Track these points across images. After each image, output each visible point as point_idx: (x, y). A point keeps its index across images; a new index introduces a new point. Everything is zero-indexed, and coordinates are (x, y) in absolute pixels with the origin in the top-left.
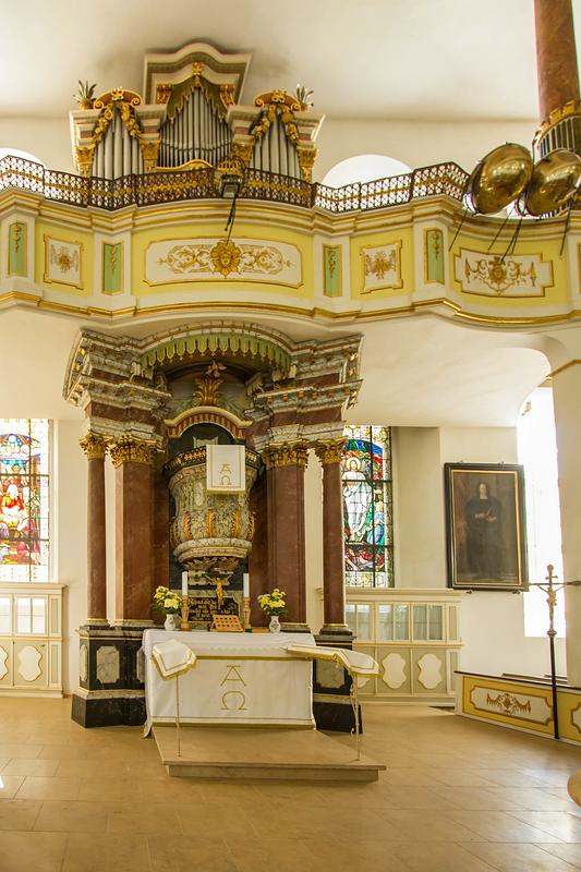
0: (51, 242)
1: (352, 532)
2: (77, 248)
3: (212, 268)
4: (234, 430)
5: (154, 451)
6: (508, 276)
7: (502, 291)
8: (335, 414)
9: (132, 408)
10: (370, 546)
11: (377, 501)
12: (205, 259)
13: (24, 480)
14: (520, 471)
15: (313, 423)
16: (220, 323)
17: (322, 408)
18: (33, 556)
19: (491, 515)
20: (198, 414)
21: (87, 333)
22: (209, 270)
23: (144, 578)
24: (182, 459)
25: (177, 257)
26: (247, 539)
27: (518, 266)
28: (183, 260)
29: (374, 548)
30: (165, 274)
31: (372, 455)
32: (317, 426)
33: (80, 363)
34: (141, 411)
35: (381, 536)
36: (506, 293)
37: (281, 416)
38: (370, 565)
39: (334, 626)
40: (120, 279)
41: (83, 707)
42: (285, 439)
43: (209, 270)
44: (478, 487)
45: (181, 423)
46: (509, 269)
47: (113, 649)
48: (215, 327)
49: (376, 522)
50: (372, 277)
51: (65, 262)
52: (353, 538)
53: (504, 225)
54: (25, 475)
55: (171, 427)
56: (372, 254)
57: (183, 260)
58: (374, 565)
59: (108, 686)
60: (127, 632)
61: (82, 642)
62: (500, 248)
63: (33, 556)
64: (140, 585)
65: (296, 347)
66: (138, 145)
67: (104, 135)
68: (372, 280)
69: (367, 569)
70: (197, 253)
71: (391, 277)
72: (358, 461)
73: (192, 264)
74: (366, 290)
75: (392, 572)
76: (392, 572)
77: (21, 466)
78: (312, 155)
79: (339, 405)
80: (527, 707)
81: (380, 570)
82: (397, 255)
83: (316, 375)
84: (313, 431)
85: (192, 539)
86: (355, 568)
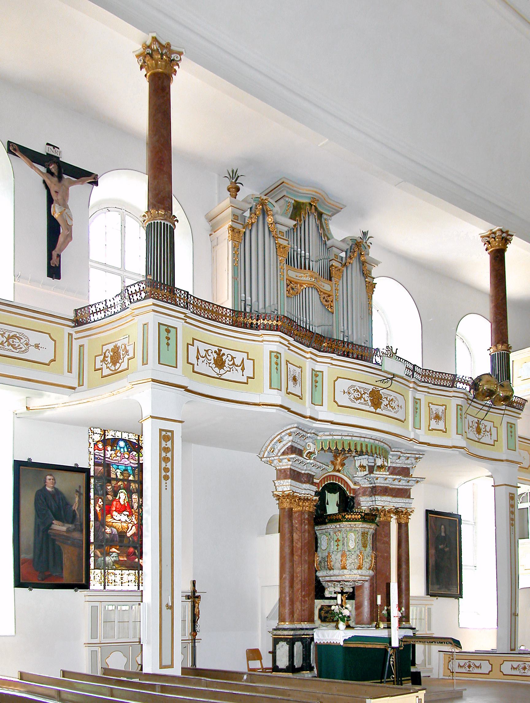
3: (370, 404)
6: (482, 431)
8: (407, 493)
12: (366, 396)
14: (460, 520)
19: (446, 546)
25: (352, 392)
28: (356, 394)
37: (380, 488)
42: (382, 504)
44: (441, 527)
50: (433, 422)
54: (134, 481)
57: (356, 394)
59: (282, 670)
79: (410, 487)
80: (479, 667)
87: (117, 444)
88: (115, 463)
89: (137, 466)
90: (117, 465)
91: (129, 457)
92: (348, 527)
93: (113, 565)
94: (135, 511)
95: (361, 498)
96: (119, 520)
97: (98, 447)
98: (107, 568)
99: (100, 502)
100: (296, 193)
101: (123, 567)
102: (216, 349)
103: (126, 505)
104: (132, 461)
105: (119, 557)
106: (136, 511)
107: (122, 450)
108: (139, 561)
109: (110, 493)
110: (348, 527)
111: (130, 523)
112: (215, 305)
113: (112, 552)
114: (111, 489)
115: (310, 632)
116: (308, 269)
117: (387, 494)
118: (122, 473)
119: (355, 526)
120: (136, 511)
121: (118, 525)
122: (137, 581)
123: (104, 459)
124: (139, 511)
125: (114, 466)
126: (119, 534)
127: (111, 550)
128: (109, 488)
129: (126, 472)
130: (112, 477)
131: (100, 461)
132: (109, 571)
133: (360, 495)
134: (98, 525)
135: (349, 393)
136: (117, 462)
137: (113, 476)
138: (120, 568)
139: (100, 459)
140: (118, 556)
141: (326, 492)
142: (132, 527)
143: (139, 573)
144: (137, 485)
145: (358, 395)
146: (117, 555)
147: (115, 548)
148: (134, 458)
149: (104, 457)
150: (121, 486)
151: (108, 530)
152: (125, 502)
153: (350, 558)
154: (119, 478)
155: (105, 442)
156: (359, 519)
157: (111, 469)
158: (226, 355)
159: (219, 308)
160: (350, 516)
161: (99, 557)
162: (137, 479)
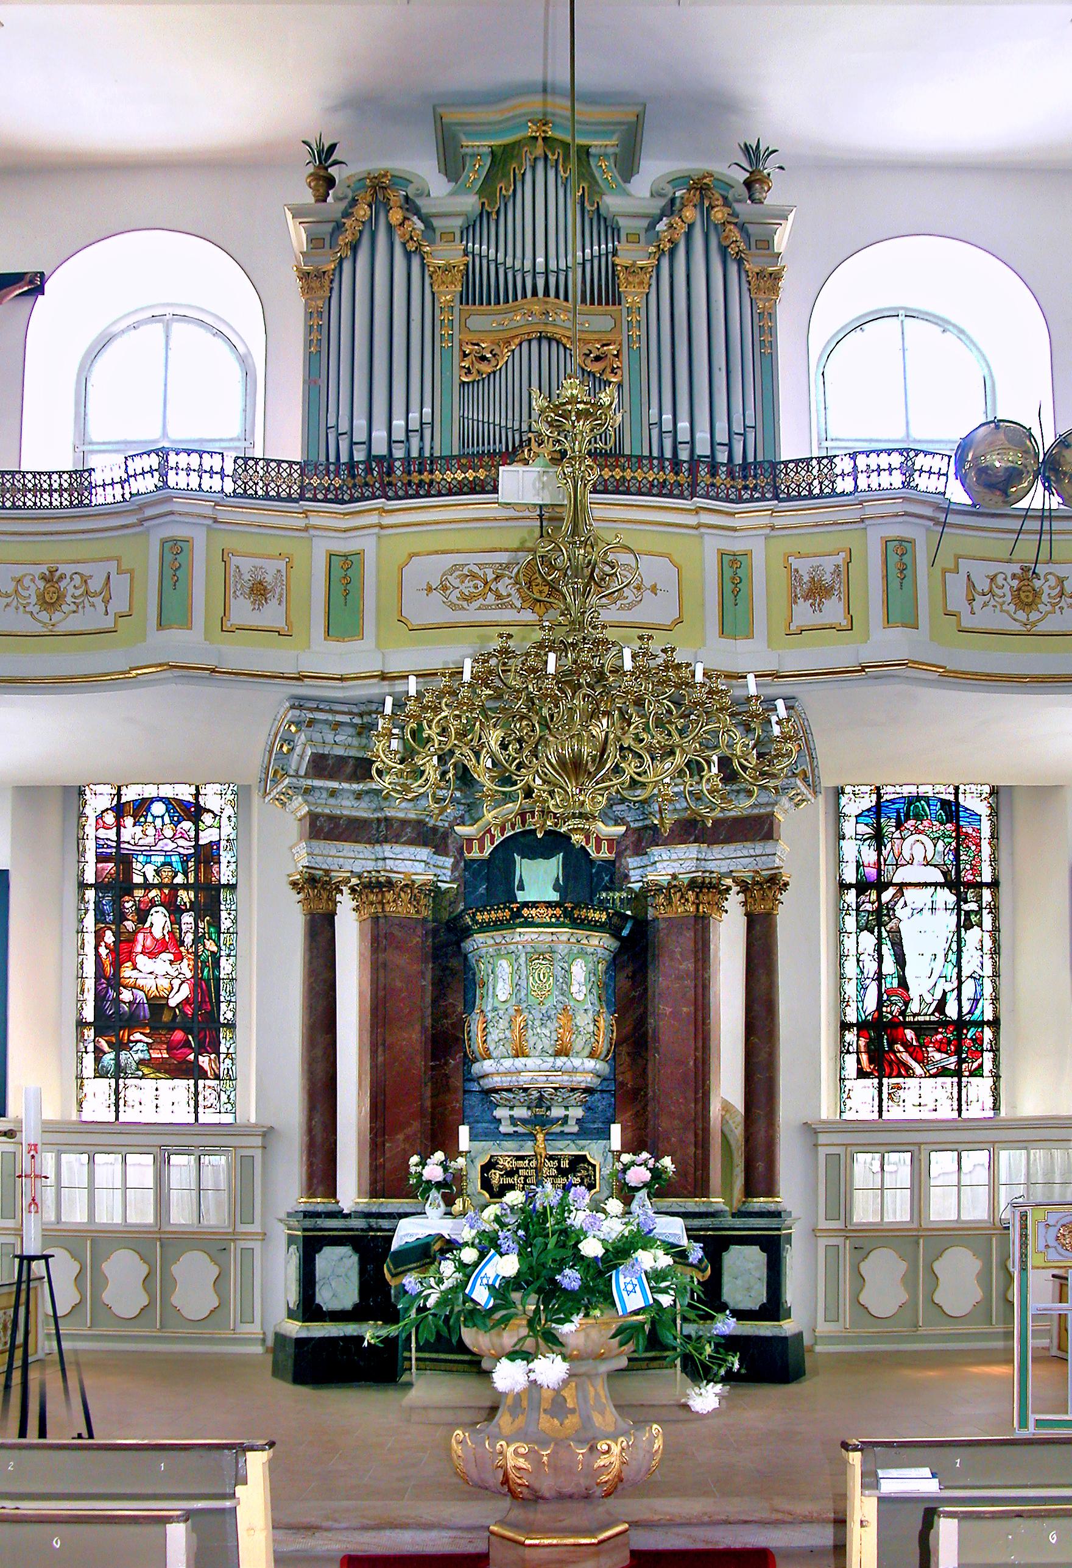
0: (235, 561)
1: (914, 993)
2: (282, 565)
4: (593, 841)
5: (435, 893)
6: (1045, 598)
7: (1034, 624)
9: (386, 819)
10: (953, 1022)
11: (969, 926)
12: (504, 586)
13: (185, 897)
15: (728, 840)
18: (204, 1061)
21: (298, 703)
22: (513, 606)
23: (409, 1124)
24: (473, 919)
26: (592, 1055)
27: (1061, 581)
28: (467, 587)
29: (961, 1024)
30: (434, 610)
31: (958, 828)
32: (732, 847)
33: (289, 742)
35: (976, 1001)
36: (1041, 628)
38: (951, 1062)
39: (759, 1203)
40: (359, 614)
41: (291, 1349)
43: (513, 606)
46: (1046, 587)
47: (346, 1250)
49: (965, 973)
50: (803, 608)
51: (259, 591)
52: (914, 1007)
53: (1026, 517)
54: (186, 887)
56: (804, 567)
57: (467, 587)
58: (961, 1062)
60: (373, 1222)
61: (291, 1240)
62: (1027, 549)
63: (204, 1061)
64: (400, 1137)
66: (423, 266)
67: (354, 248)
68: (804, 613)
69: (943, 1072)
70: (490, 576)
71: (833, 610)
72: (929, 844)
73: (484, 596)
74: (793, 628)
75: (997, 1077)
76: (997, 1077)
77: (178, 866)
78: (776, 277)
79: (769, 809)
81: (972, 1074)
82: (844, 576)
84: (727, 855)
85: (490, 1057)
86: (919, 1070)
87: (148, 809)
88: (142, 851)
89: (192, 851)
90: (147, 856)
91: (175, 835)
92: (490, 946)
93: (138, 1069)
94: (187, 950)
95: (629, 860)
96: (151, 973)
97: (104, 822)
98: (122, 1075)
99: (109, 938)
100: (476, 128)
101: (160, 1073)
102: (44, 569)
103: (167, 940)
104: (181, 842)
105: (151, 1051)
106: (190, 951)
107: (158, 822)
108: (196, 1058)
109: (130, 917)
110: (490, 946)
111: (177, 977)
112: (272, 460)
113: (133, 1042)
114: (133, 908)
115: (385, 1223)
116: (544, 296)
117: (692, 839)
118: (158, 872)
119: (504, 942)
120: (190, 951)
121: (148, 983)
122: (192, 1103)
123: (118, 847)
124: (197, 949)
125: (141, 858)
126: (151, 1002)
127: (132, 1038)
128: (127, 905)
129: (167, 868)
130: (134, 881)
131: (109, 851)
132: (127, 1081)
133: (628, 852)
134: (104, 985)
135: (445, 588)
136: (148, 848)
137: (137, 879)
138: (152, 1076)
139: (109, 847)
140: (148, 1050)
141: (517, 858)
142: (180, 985)
143: (196, 1086)
144: (193, 893)
145: (476, 587)
146: (145, 1048)
147: (141, 1033)
148: (186, 836)
149: (119, 842)
150: (156, 899)
151: (126, 995)
152: (165, 932)
153: (495, 1028)
154: (151, 882)
155: (120, 810)
156: (506, 920)
157: (134, 864)
158: (68, 577)
159: (38, 476)
160: (486, 916)
161: (105, 1053)
162: (191, 881)
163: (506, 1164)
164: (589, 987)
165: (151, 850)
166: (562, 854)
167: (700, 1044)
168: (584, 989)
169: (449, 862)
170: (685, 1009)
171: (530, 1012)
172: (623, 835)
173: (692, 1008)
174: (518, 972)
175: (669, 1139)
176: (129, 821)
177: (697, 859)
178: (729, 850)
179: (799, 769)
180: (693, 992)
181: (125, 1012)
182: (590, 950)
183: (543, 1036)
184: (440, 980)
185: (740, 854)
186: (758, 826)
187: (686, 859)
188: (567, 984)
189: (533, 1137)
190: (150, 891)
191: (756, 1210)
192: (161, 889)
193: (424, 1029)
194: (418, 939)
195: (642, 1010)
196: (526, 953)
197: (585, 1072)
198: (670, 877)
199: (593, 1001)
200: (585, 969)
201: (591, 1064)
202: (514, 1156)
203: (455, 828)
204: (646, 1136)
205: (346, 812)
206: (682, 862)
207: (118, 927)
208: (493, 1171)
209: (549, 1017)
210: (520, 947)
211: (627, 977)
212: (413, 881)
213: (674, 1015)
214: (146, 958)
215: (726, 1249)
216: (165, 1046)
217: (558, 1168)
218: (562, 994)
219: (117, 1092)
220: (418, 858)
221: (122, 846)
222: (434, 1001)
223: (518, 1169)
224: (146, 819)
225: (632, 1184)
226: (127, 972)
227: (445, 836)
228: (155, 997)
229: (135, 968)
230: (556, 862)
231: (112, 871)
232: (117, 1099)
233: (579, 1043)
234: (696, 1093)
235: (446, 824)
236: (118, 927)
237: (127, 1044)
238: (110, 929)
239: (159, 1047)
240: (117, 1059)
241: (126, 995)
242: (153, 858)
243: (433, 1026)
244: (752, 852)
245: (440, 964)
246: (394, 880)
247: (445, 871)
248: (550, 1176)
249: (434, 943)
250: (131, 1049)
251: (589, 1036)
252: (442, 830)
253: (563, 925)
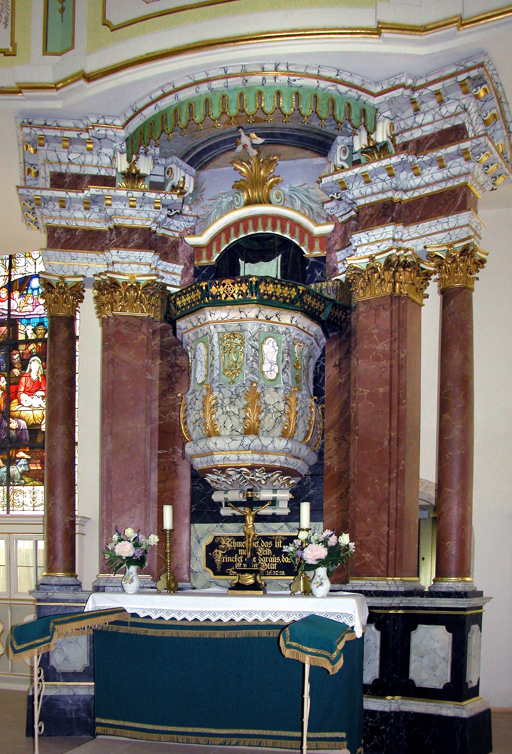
8: (455, 199)
15: (424, 218)
16: (222, 72)
17: (436, 188)
20: (244, 221)
32: (426, 224)
34: (132, 230)
45: (216, 238)
48: (215, 79)
55: (197, 248)
65: (379, 89)
83: (428, 130)
84: (421, 232)
87: (29, 285)
90: (28, 319)
98: (11, 483)
101: (36, 481)
103: (40, 381)
105: (30, 465)
109: (16, 366)
113: (18, 459)
118: (34, 331)
123: (9, 314)
125: (24, 321)
127: (17, 456)
129: (41, 328)
130: (19, 339)
132: (15, 488)
136: (28, 313)
137: (21, 337)
140: (28, 464)
141: (241, 262)
147: (24, 452)
149: (9, 310)
150: (33, 351)
151: (14, 424)
153: (192, 410)
157: (19, 326)
163: (228, 544)
164: (282, 367)
165: (30, 315)
166: (280, 256)
167: (394, 424)
168: (276, 368)
169: (179, 268)
170: (381, 390)
171: (220, 392)
172: (333, 231)
173: (388, 388)
174: (212, 353)
175: (365, 521)
176: (16, 294)
177: (394, 240)
178: (424, 227)
179: (489, 115)
180: (388, 372)
181: (13, 437)
182: (282, 329)
183: (232, 414)
184: (169, 376)
185: (434, 230)
186: (452, 200)
187: (383, 240)
188: (257, 362)
189: (242, 519)
190: (30, 345)
191: (443, 590)
192: (36, 343)
193: (149, 420)
194: (143, 336)
195: (346, 396)
196: (218, 333)
197: (276, 452)
198: (368, 260)
199: (286, 381)
200: (277, 348)
201: (281, 444)
202: (235, 537)
203: (186, 239)
204: (348, 517)
205: (81, 224)
206: (379, 244)
207: (9, 374)
208: (216, 551)
209: (238, 395)
210: (212, 327)
211: (335, 366)
212: (138, 283)
213: (371, 396)
214: (27, 395)
215: (415, 628)
216: (39, 461)
217: (273, 548)
218: (253, 373)
219: (8, 497)
220: (143, 261)
221: (12, 313)
222: (163, 395)
223: (238, 548)
224: (27, 292)
225: (309, 562)
226: (14, 406)
227: (175, 245)
228: (33, 424)
229: (20, 403)
230: (275, 264)
231: (5, 332)
232: (8, 501)
233: (268, 421)
234: (390, 473)
235: (177, 235)
236: (9, 374)
237: (15, 460)
238: (4, 376)
239: (35, 461)
240: (8, 471)
241: (14, 424)
242: (32, 321)
243: (160, 418)
244: (446, 226)
245: (169, 361)
246: (120, 282)
247: (175, 277)
248: (265, 556)
249: (162, 342)
250: (17, 463)
251: (279, 414)
252: (172, 239)
253: (250, 302)
